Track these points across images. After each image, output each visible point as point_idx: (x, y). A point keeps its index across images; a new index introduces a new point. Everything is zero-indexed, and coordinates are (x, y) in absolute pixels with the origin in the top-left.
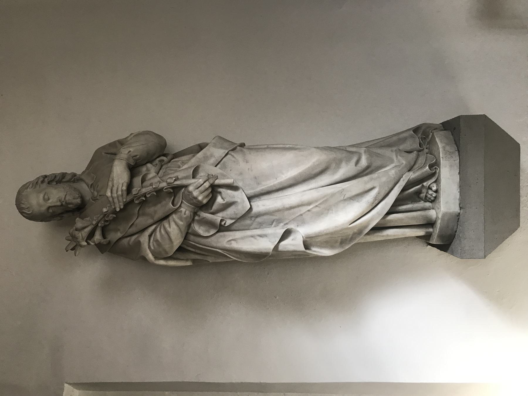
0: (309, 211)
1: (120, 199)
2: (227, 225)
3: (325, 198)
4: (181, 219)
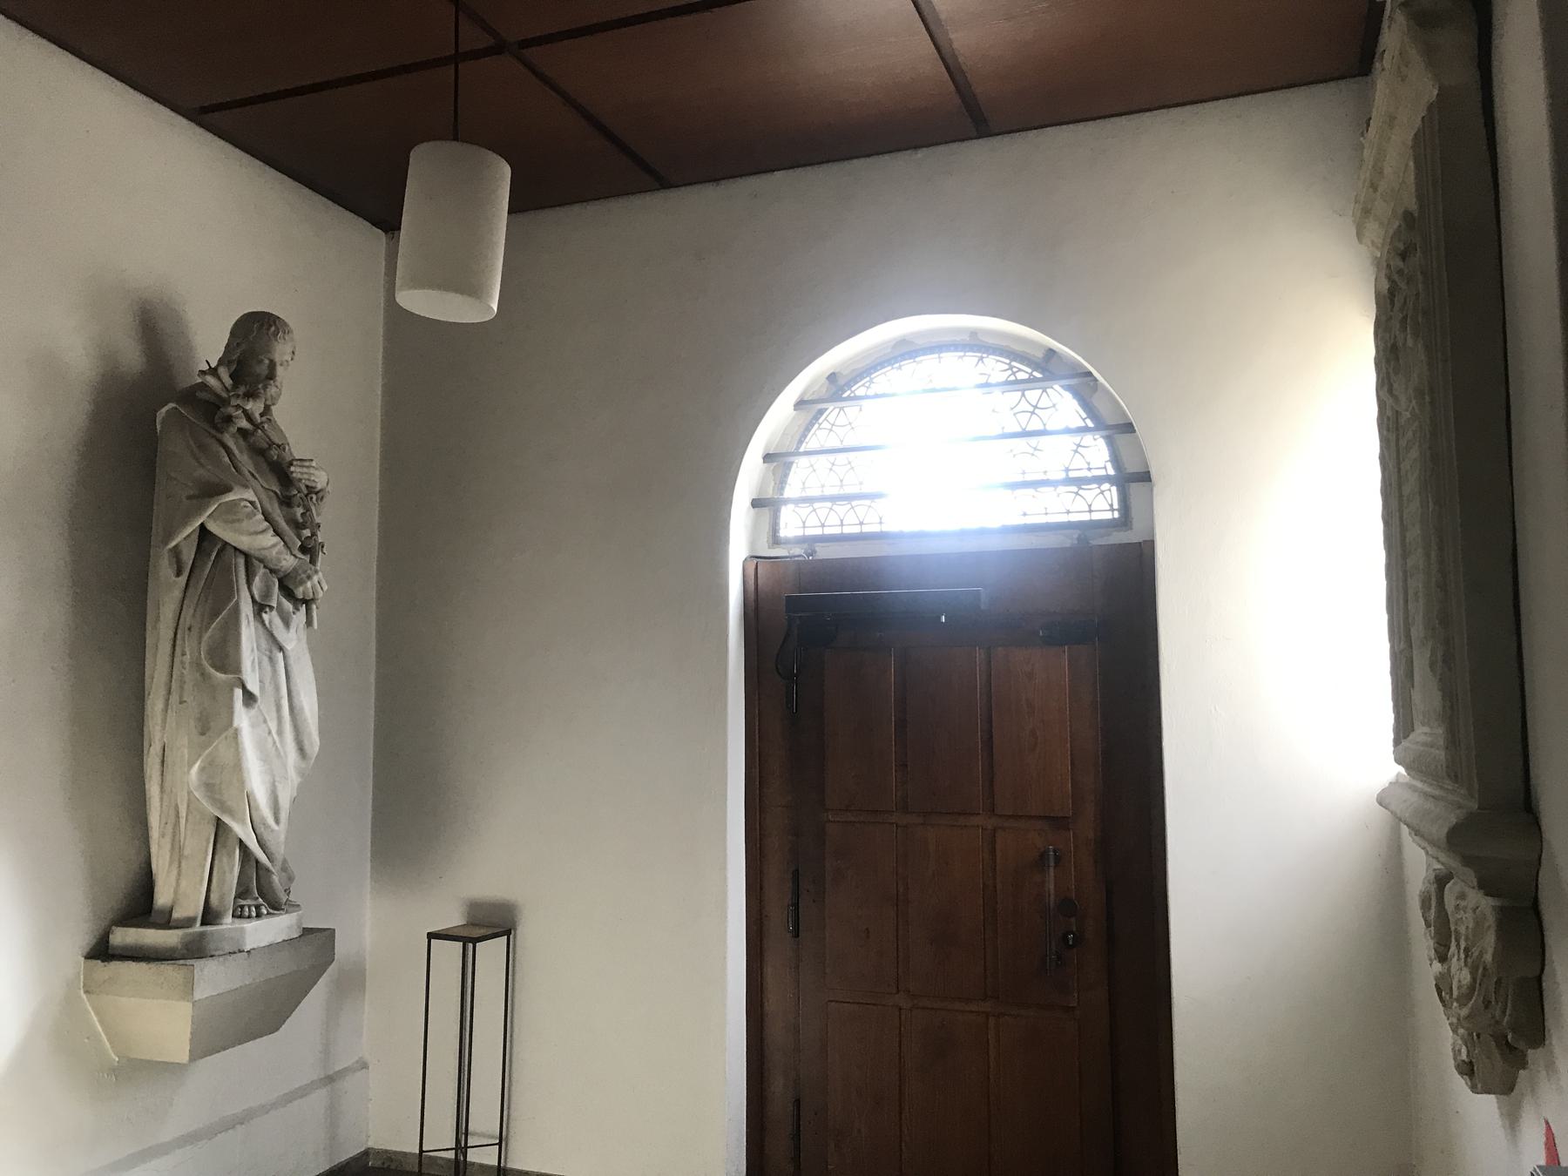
0: (270, 733)
1: (306, 476)
2: (264, 615)
3: (282, 754)
4: (279, 553)
